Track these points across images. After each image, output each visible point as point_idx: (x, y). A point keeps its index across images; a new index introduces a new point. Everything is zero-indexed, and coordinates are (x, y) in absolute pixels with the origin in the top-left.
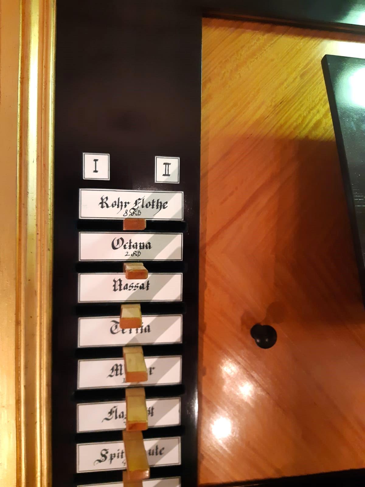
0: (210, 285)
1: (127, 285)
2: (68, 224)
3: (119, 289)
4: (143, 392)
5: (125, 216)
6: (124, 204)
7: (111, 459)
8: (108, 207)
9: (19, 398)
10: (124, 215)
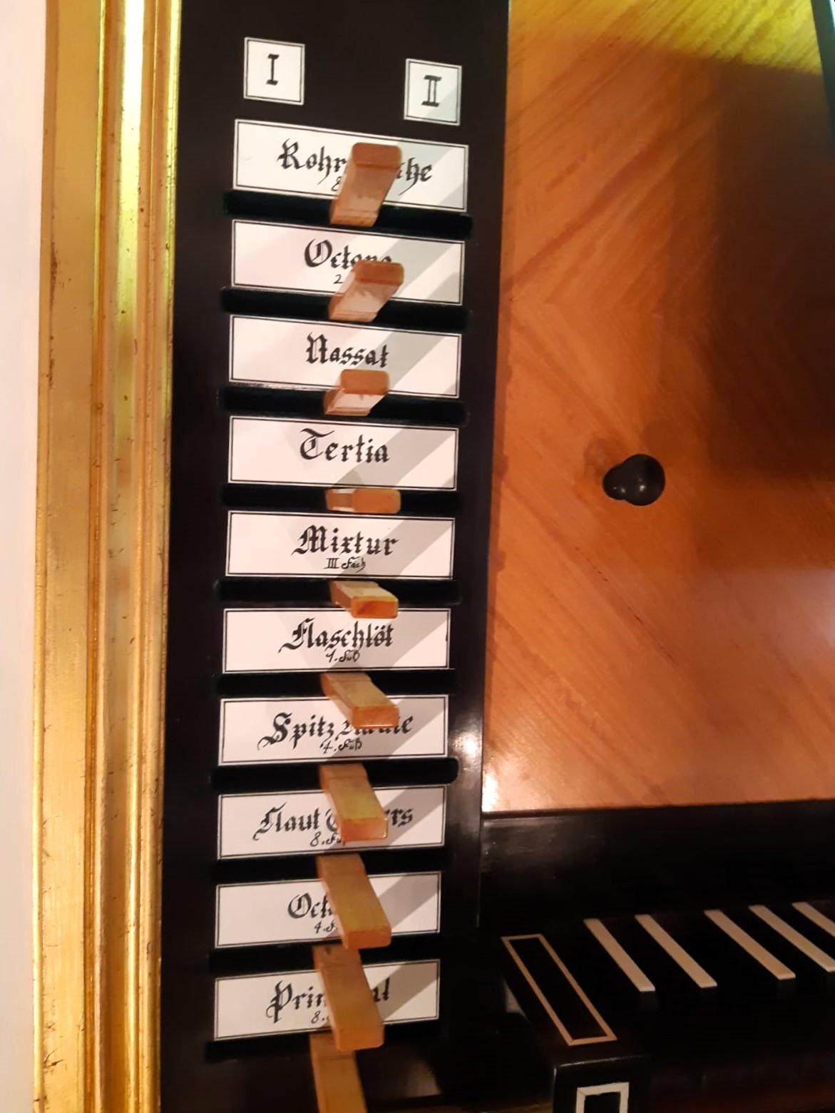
0: (518, 372)
1: (337, 350)
2: (209, 202)
3: (319, 360)
4: (358, 864)
5: (335, 190)
6: (333, 164)
7: (297, 737)
8: (297, 166)
9: (93, 762)
10: (334, 188)
